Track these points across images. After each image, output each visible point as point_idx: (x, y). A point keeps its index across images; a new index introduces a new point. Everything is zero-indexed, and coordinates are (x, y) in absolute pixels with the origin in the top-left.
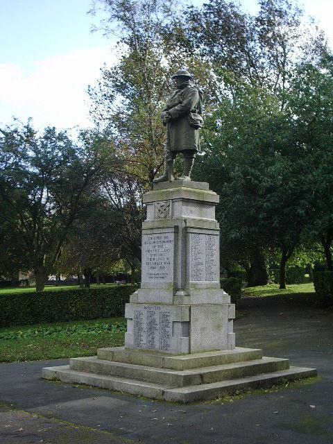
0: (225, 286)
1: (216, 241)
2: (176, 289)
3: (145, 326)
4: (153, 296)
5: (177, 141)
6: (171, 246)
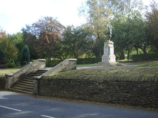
0: (114, 54)
1: (113, 48)
2: (108, 54)
3: (104, 59)
4: (106, 55)
5: (108, 36)
6: (108, 49)
